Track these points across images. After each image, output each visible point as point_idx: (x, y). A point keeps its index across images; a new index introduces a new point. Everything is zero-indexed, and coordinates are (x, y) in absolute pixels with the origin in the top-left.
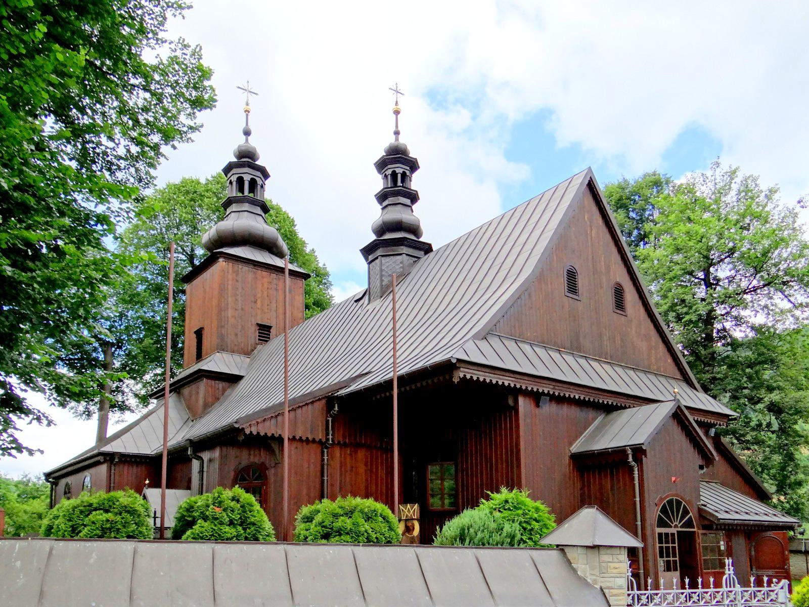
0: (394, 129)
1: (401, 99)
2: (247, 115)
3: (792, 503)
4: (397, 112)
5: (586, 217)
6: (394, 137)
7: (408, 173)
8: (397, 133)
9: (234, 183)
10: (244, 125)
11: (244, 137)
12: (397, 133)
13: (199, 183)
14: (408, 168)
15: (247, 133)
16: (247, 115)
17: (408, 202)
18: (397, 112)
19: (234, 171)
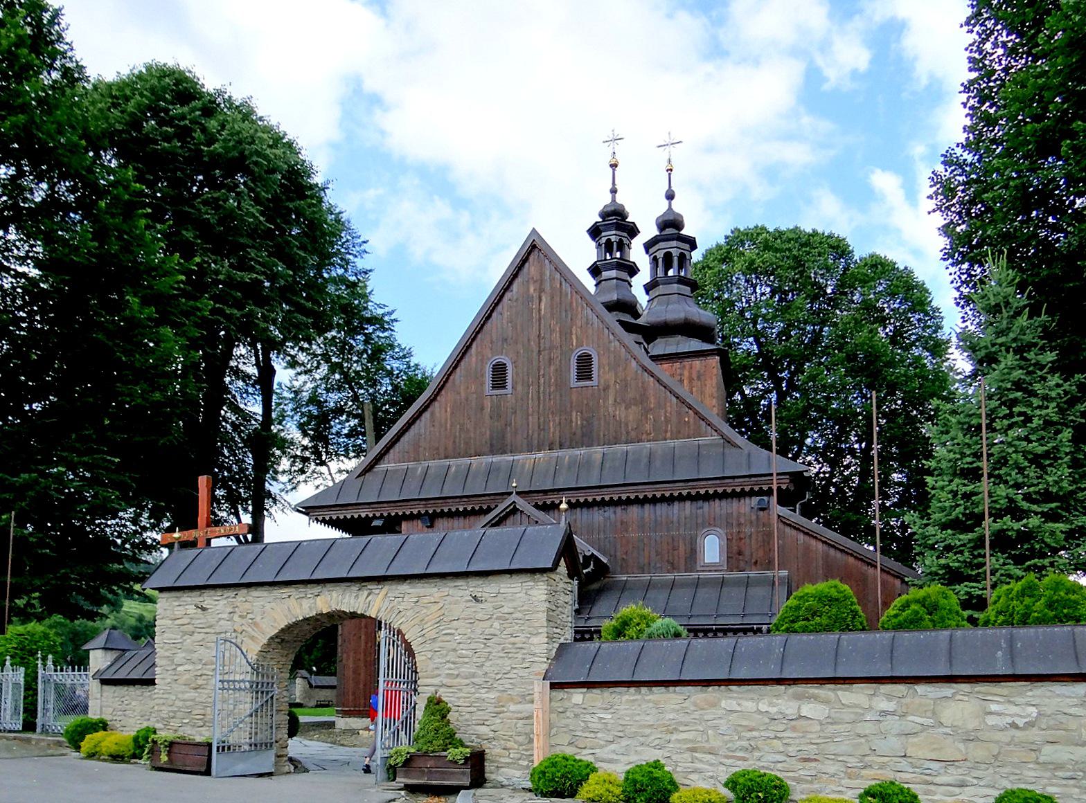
0: (611, 186)
1: (620, 148)
2: (614, 170)
3: (602, 536)
4: (614, 166)
5: (169, 129)
6: (610, 196)
7: (625, 241)
8: (614, 191)
9: (660, 261)
10: (667, 188)
11: (667, 202)
12: (614, 191)
13: (309, 177)
14: (626, 235)
15: (670, 196)
16: (614, 170)
17: (624, 275)
18: (614, 166)
19: (662, 245)
